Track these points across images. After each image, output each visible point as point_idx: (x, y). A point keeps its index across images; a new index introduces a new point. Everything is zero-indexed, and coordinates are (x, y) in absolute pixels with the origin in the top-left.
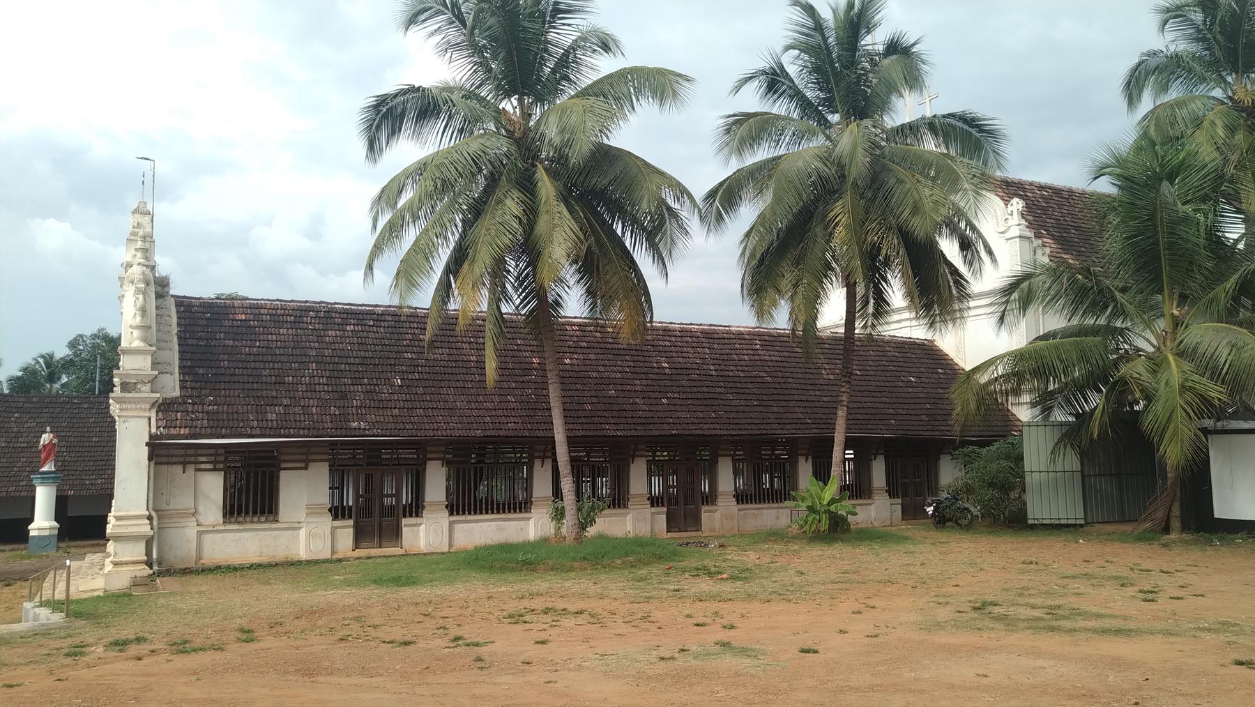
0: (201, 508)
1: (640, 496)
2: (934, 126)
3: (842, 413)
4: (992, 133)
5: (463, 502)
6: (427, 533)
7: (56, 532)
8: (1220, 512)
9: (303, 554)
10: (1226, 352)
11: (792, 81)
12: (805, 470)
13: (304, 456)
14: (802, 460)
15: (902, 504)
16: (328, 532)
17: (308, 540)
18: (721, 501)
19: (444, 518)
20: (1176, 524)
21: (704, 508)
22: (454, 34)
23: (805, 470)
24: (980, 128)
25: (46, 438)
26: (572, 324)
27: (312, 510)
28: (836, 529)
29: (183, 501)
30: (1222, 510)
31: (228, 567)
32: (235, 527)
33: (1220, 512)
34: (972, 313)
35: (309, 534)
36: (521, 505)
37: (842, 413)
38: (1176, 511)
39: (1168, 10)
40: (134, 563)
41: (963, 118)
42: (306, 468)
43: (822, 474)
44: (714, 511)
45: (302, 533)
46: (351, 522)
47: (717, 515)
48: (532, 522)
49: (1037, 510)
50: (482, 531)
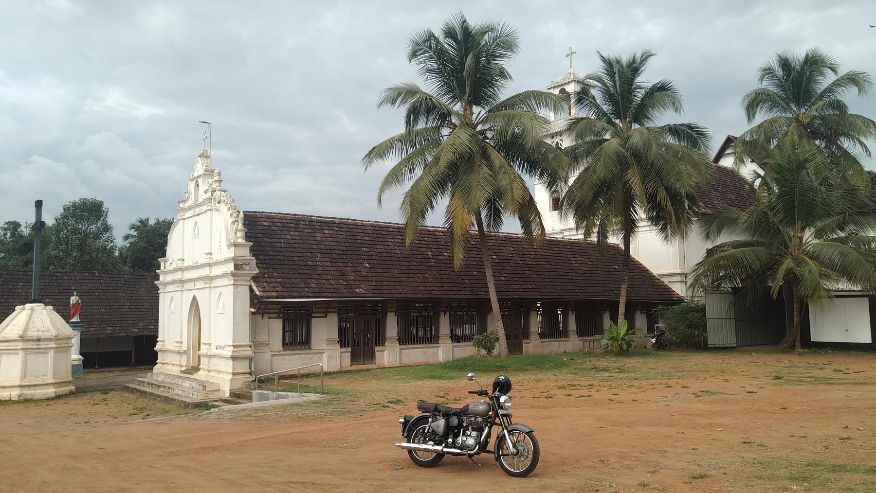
0: (271, 341)
1: (446, 335)
2: (674, 130)
3: (624, 286)
4: (703, 135)
5: (406, 339)
6: (389, 354)
7: (81, 362)
8: (813, 338)
9: (325, 369)
10: (838, 257)
11: (594, 99)
12: (606, 318)
13: (325, 309)
14: (570, 313)
15: (352, 352)
16: (338, 355)
17: (328, 360)
18: (571, 336)
19: (396, 346)
20: (798, 344)
21: (524, 341)
22: (432, 65)
23: (606, 318)
24: (698, 133)
25: (73, 299)
26: (439, 232)
27: (329, 342)
28: (625, 350)
29: (263, 337)
30: (816, 336)
31: (314, 374)
32: (290, 352)
33: (813, 338)
34: (640, 229)
35: (329, 357)
36: (432, 339)
37: (624, 286)
38: (798, 338)
39: (765, 70)
40: (244, 373)
41: (689, 127)
42: (326, 317)
43: (614, 319)
44: (384, 351)
45: (325, 356)
46: (350, 349)
47: (531, 345)
48: (440, 349)
49: (713, 338)
50: (416, 354)
